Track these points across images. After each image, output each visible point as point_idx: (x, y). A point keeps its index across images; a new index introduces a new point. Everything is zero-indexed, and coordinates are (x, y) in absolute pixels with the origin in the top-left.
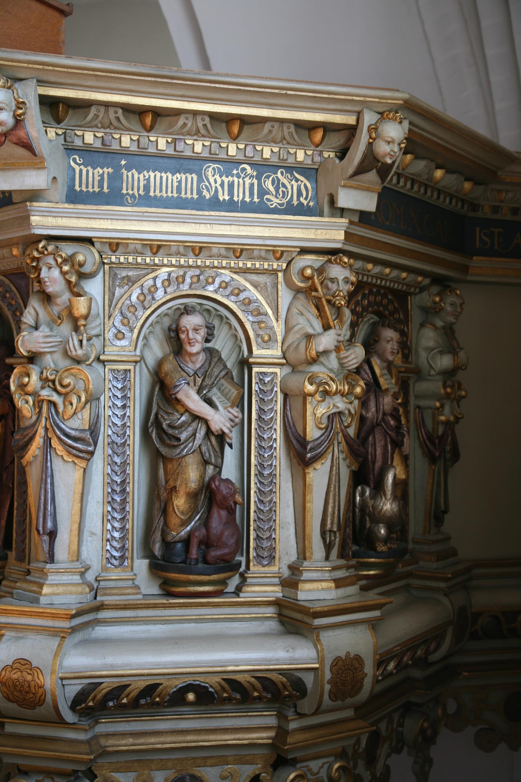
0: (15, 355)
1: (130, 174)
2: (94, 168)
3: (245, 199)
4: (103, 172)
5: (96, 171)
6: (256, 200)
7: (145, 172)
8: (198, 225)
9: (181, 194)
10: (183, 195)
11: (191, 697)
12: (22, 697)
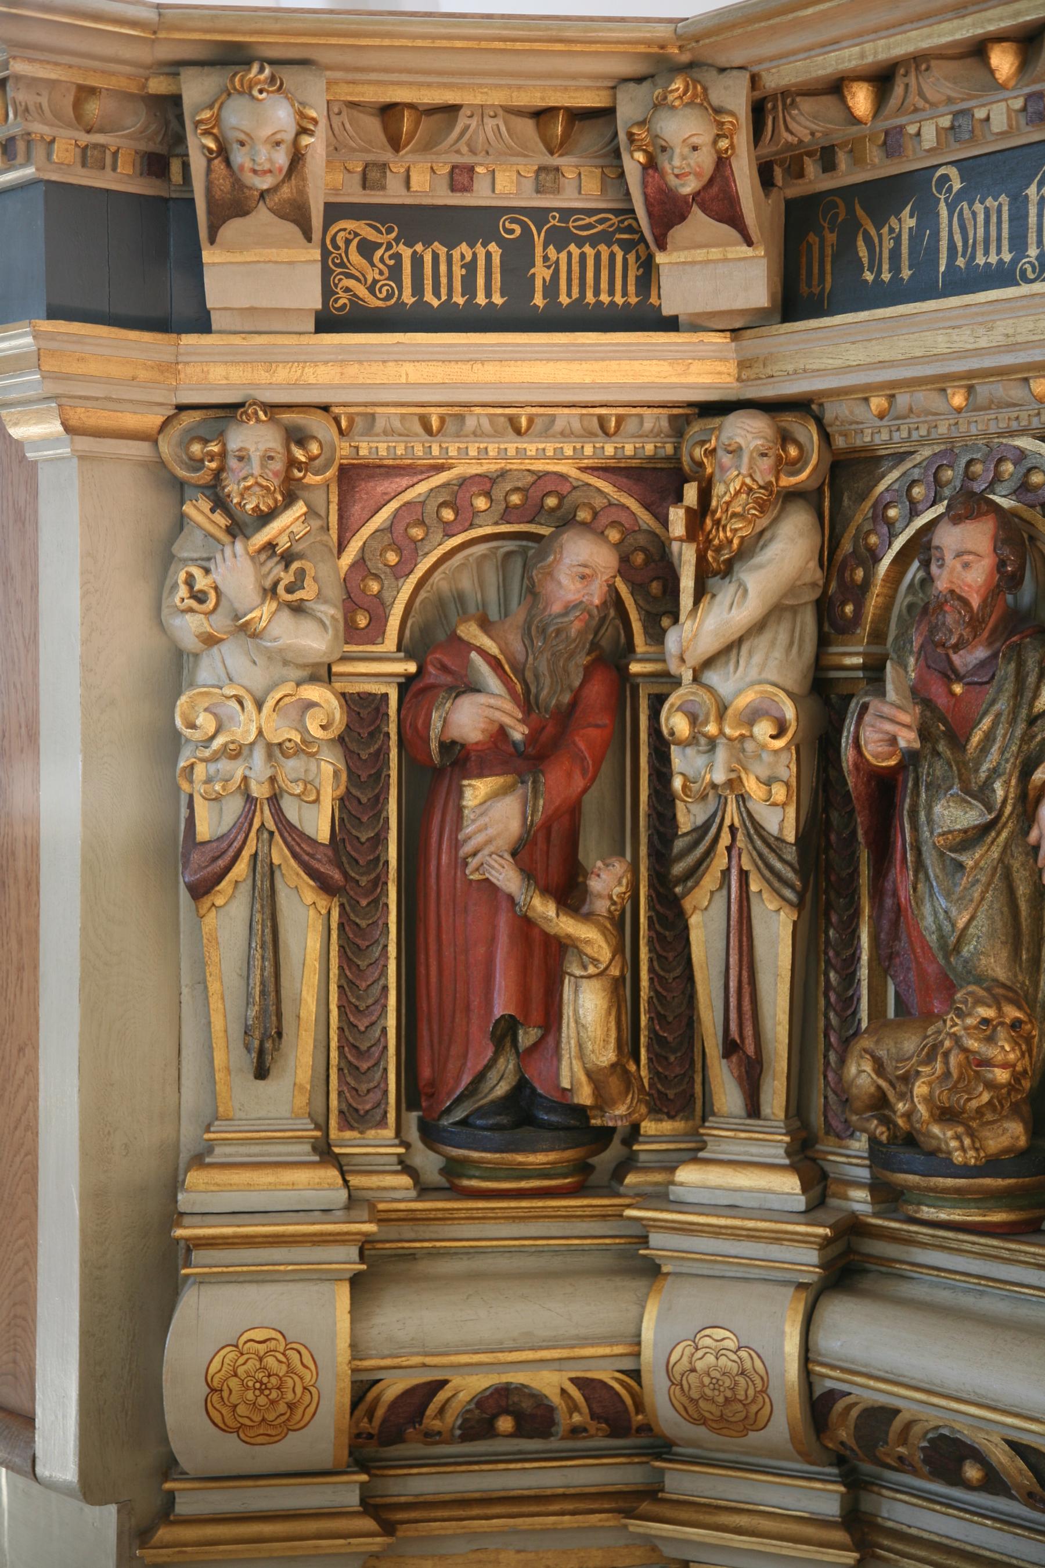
0: (402, 680)
1: (563, 255)
2: (451, 246)
3: (454, 299)
4: (475, 255)
5: (456, 254)
6: (633, 300)
7: (572, 247)
8: (468, 366)
9: (474, 295)
10: (481, 299)
11: (505, 1424)
12: (257, 1418)
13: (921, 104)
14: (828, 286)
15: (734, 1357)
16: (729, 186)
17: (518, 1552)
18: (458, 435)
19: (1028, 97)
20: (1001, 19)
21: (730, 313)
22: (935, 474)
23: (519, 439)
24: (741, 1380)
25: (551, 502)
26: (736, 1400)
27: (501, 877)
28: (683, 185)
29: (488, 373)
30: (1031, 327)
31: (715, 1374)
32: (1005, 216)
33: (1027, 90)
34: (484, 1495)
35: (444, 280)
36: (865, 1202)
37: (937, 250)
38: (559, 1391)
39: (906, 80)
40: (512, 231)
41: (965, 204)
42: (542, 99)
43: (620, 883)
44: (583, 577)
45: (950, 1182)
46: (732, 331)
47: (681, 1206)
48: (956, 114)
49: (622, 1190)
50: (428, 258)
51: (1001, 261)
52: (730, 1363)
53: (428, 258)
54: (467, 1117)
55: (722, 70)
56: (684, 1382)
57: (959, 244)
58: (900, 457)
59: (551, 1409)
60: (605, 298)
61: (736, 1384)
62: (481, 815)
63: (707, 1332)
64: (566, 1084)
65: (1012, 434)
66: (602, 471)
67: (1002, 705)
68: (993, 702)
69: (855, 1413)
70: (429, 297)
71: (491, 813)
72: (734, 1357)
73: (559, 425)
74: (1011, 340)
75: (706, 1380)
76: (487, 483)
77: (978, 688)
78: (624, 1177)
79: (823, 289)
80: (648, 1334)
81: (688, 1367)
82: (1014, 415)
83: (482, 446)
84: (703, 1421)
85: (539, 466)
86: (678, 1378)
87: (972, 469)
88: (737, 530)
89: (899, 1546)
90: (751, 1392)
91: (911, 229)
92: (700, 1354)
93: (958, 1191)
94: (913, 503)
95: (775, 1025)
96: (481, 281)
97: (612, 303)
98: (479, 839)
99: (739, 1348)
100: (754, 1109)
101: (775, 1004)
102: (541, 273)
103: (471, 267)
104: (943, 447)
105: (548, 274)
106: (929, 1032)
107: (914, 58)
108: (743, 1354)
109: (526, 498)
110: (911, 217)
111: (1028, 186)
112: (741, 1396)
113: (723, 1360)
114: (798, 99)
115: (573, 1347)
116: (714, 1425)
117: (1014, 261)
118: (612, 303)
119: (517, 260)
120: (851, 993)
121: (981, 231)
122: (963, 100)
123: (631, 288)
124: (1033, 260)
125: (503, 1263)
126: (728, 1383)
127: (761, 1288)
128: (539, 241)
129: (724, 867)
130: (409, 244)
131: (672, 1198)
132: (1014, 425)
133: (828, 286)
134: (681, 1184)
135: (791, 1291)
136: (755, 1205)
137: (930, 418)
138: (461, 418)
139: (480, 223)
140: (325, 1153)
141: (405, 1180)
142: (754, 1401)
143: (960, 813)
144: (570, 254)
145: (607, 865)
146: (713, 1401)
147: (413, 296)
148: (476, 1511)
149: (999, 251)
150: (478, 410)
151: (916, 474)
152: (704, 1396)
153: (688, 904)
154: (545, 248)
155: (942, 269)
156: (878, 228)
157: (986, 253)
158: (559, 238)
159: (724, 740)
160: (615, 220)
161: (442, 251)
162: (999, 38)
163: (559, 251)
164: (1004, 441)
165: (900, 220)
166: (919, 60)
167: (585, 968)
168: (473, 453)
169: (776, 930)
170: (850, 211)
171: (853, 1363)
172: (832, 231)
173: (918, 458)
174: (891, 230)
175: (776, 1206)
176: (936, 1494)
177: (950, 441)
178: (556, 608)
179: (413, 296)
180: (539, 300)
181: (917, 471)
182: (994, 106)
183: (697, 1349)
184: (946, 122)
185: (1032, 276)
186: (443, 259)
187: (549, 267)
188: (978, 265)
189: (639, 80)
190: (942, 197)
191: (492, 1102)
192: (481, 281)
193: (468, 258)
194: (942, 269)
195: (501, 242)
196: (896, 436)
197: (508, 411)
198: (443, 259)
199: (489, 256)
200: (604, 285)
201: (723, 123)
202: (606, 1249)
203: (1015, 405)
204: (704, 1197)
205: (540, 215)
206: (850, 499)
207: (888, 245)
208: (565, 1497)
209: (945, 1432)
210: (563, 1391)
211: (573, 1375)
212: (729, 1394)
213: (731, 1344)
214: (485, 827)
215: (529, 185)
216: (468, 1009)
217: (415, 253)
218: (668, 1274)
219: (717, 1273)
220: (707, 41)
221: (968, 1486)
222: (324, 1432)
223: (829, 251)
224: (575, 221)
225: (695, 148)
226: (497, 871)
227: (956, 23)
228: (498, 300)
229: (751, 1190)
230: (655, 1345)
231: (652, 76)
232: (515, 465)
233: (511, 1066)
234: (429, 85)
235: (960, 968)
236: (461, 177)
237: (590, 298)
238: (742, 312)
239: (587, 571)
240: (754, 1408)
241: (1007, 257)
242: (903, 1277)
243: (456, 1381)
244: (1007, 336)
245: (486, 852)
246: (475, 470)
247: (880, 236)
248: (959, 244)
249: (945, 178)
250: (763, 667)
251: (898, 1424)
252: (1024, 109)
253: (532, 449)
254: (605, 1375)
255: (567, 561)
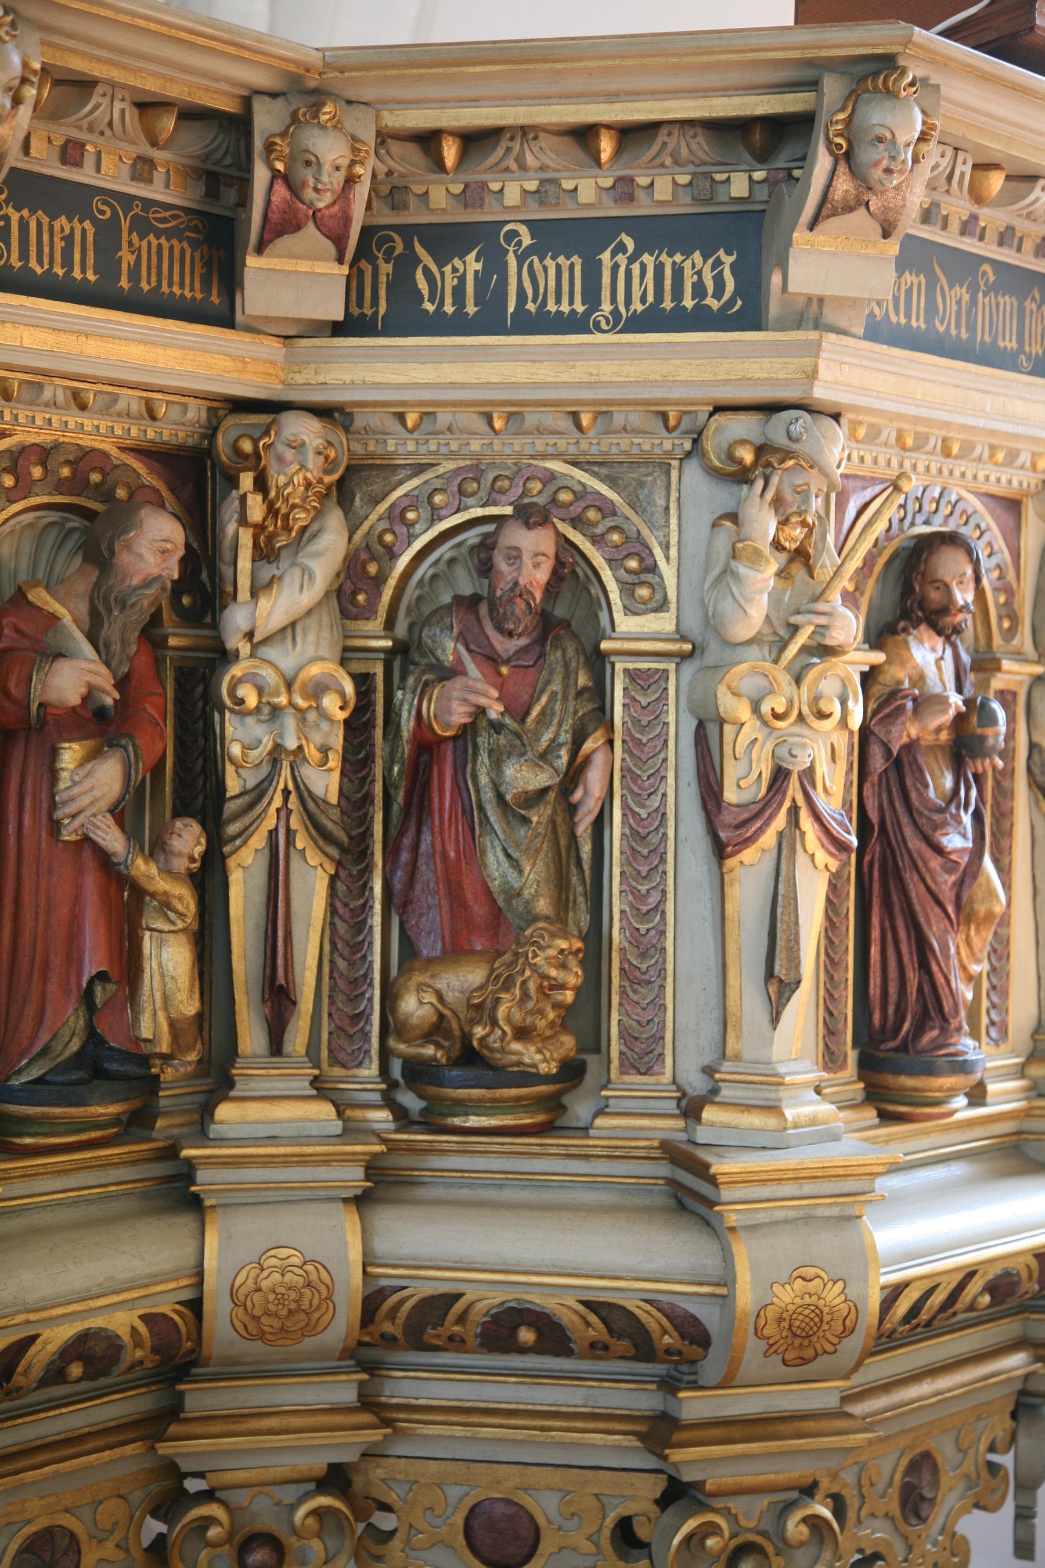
1: (144, 243)
2: (53, 218)
4: (72, 229)
5: (57, 225)
7: (151, 237)
8: (74, 338)
9: (71, 269)
11: (76, 1370)
13: (514, 166)
14: (382, 310)
15: (300, 1272)
16: (349, 206)
17: (42, 1498)
18: (32, 403)
19: (619, 180)
20: (651, 112)
21: (286, 320)
22: (460, 486)
23: (80, 413)
24: (307, 1292)
25: (95, 477)
26: (299, 1310)
27: (108, 838)
28: (319, 200)
29: (91, 347)
30: (616, 369)
31: (280, 1290)
32: (923, 287)
33: (620, 173)
34: (22, 1447)
35: (46, 250)
36: (387, 1121)
37: (506, 295)
38: (129, 1329)
39: (511, 144)
40: (103, 213)
41: (536, 259)
42: (189, 94)
43: (199, 843)
44: (163, 552)
45: (513, 1092)
46: (286, 337)
47: (222, 1141)
48: (543, 182)
49: (154, 1134)
50: (33, 225)
51: (573, 312)
52: (296, 1278)
53: (33, 225)
54: (45, 1074)
55: (349, 102)
56: (249, 1304)
57: (530, 292)
58: (419, 469)
59: (120, 1348)
60: (176, 289)
61: (301, 1295)
62: (86, 776)
63: (272, 1253)
64: (146, 1033)
65: (544, 457)
66: (138, 451)
67: (556, 686)
68: (548, 682)
69: (409, 1305)
70: (33, 264)
71: (97, 775)
72: (301, 1272)
73: (121, 405)
74: (593, 379)
75: (271, 1297)
76: (44, 454)
77: (523, 670)
78: (155, 1122)
79: (376, 313)
80: (210, 1263)
81: (253, 1287)
82: (552, 442)
83: (47, 416)
84: (261, 1336)
85: (87, 442)
86: (242, 1299)
87: (499, 484)
88: (301, 518)
89: (417, 1417)
90: (316, 1301)
91: (476, 272)
92: (265, 1273)
93: (518, 1099)
94: (434, 508)
95: (304, 970)
96: (77, 256)
97: (182, 295)
98: (86, 800)
99: (305, 1263)
100: (276, 1046)
101: (306, 950)
102: (127, 258)
103: (69, 240)
104: (468, 462)
105: (132, 258)
106: (496, 965)
107: (522, 127)
108: (309, 1267)
109: (74, 472)
110: (477, 260)
111: (602, 252)
112: (305, 1305)
113: (289, 1276)
114: (389, 141)
115: (147, 1286)
116: (271, 1338)
117: (587, 314)
118: (193, 298)
119: (107, 239)
120: (361, 938)
121: (552, 284)
122: (555, 170)
123: (197, 285)
124: (607, 314)
125: (48, 1217)
126: (293, 1295)
127: (312, 1207)
128: (125, 225)
129: (272, 827)
130: (18, 209)
131: (211, 1136)
132: (550, 450)
133: (382, 310)
134: (221, 1122)
135: (341, 1205)
136: (294, 1133)
137: (465, 436)
138: (40, 386)
139: (72, 199)
140: (321, 1088)
141: (325, 1110)
142: (318, 1308)
143: (531, 775)
144: (149, 243)
145: (186, 826)
146: (276, 1315)
147: (20, 260)
148: (21, 1464)
149: (571, 302)
150: (58, 381)
151: (438, 484)
152: (267, 1313)
153: (231, 863)
154: (130, 234)
155: (511, 309)
156: (441, 265)
157: (558, 301)
158: (141, 226)
159: (292, 711)
160: (185, 218)
161: (45, 220)
162: (608, 127)
163: (141, 239)
164: (535, 462)
165: (464, 263)
166: (526, 132)
167: (173, 923)
168: (39, 422)
169: (312, 885)
170: (409, 245)
171: (415, 1259)
172: (387, 261)
173: (441, 470)
174: (455, 270)
175: (314, 1133)
176: (445, 1366)
177: (477, 457)
178: (136, 581)
179: (20, 260)
180: (124, 283)
181: (440, 481)
182: (583, 181)
183: (262, 1270)
184: (532, 186)
185: (606, 328)
186: (45, 228)
187: (133, 253)
188: (549, 312)
189: (274, 95)
190: (511, 249)
191: (69, 1058)
192: (77, 256)
193: (67, 232)
194: (511, 309)
195: (95, 222)
196: (423, 449)
197: (76, 384)
198: (45, 228)
199: (84, 231)
200: (176, 278)
201: (359, 150)
202: (128, 1194)
203: (559, 433)
204: (244, 1132)
205: (126, 200)
206: (362, 500)
207: (450, 282)
208: (90, 1435)
209: (514, 1305)
210: (134, 1329)
211: (142, 1312)
212: (293, 1306)
213: (297, 1261)
214: (91, 789)
215: (125, 170)
216: (46, 965)
217: (22, 218)
218: (213, 1207)
219: (260, 1200)
220: (354, 74)
221: (523, 1350)
222: (343, 1322)
223: (383, 279)
224: (155, 212)
225: (338, 169)
226: (104, 831)
227: (603, 106)
228: (91, 277)
229: (289, 1121)
230: (219, 1272)
231: (284, 94)
232: (69, 438)
233: (81, 1022)
234: (99, 59)
235: (521, 908)
236: (71, 153)
237: (165, 288)
238: (297, 321)
239: (169, 546)
240: (317, 1315)
241: (580, 308)
242: (412, 1183)
243: (46, 1334)
244: (591, 374)
245: (88, 813)
246: (32, 439)
247: (442, 274)
248: (530, 292)
249: (513, 234)
250: (317, 644)
251: (459, 1307)
252: (613, 187)
253: (89, 424)
254: (165, 1308)
255: (150, 535)
